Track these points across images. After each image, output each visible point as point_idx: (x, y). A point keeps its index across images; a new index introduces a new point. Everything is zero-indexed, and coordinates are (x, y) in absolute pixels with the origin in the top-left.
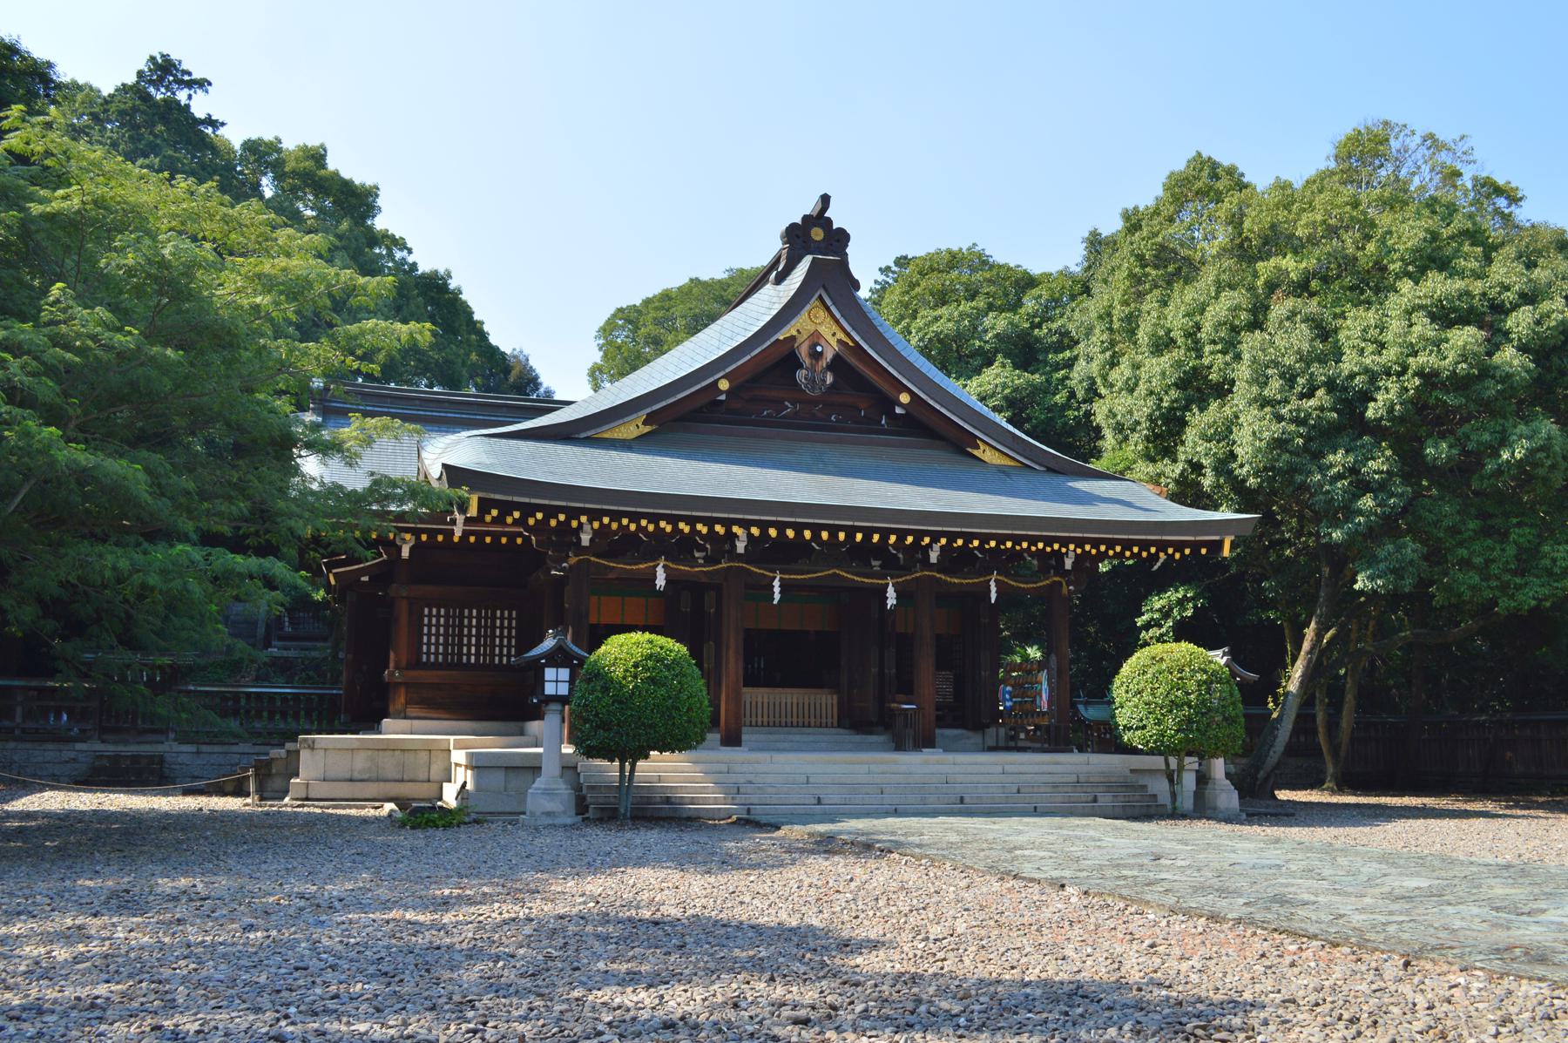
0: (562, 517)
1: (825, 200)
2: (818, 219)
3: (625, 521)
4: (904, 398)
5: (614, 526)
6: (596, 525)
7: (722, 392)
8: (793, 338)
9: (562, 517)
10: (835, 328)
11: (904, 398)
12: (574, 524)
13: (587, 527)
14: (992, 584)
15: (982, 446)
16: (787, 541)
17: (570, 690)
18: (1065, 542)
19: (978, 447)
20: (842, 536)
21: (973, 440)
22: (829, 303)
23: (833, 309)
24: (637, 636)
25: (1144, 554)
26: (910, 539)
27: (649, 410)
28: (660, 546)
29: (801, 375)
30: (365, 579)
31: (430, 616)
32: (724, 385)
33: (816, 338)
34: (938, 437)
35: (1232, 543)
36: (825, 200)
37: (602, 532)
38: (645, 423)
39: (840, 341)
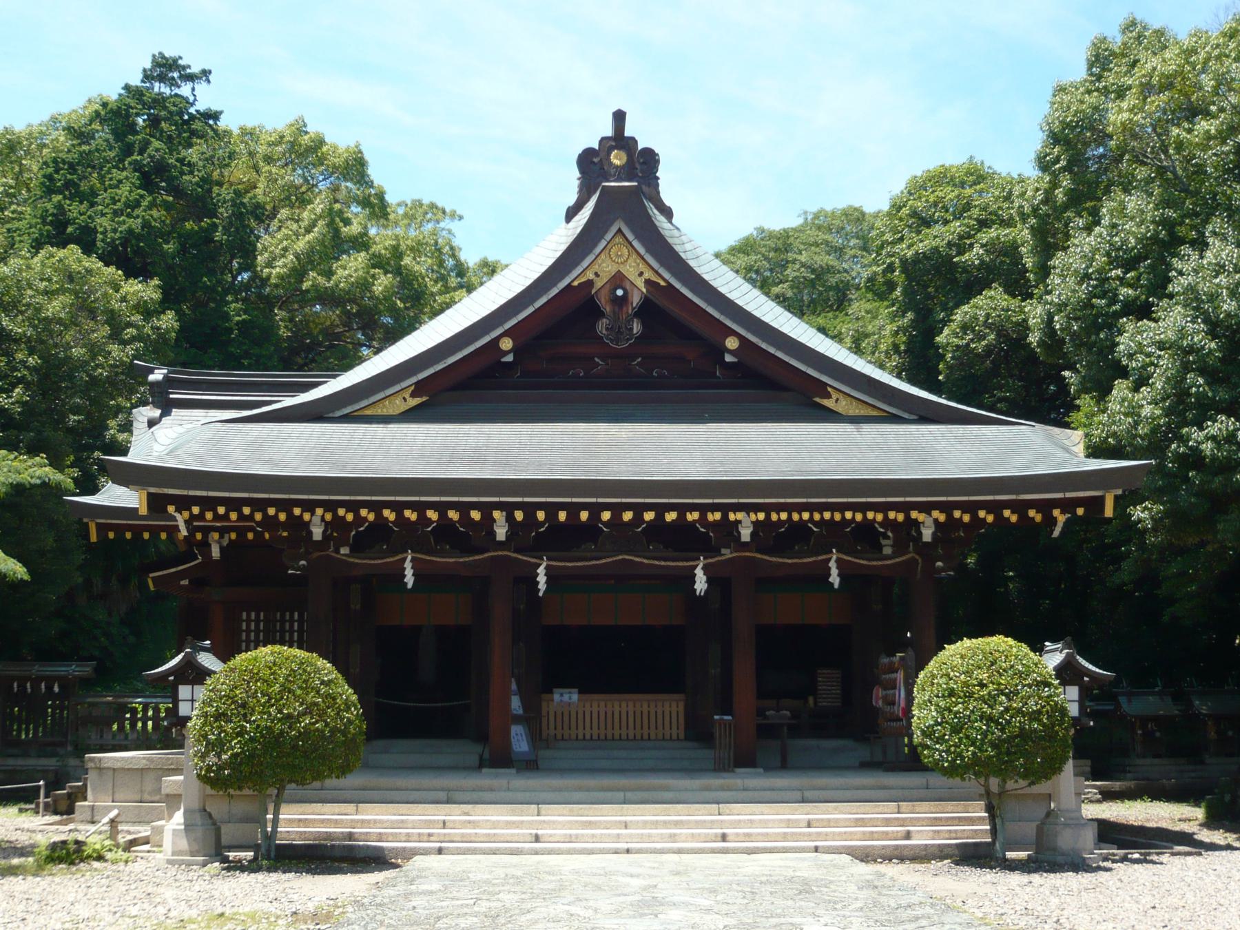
1: (619, 117)
2: (619, 139)
3: (271, 511)
4: (732, 343)
7: (506, 353)
8: (590, 283)
10: (642, 267)
11: (732, 343)
14: (832, 564)
15: (835, 395)
16: (564, 523)
18: (310, 506)
19: (829, 396)
20: (541, 515)
21: (822, 389)
22: (630, 237)
23: (636, 244)
27: (414, 380)
28: (834, 534)
29: (602, 326)
30: (185, 582)
31: (249, 621)
32: (507, 344)
33: (618, 279)
34: (777, 385)
35: (1117, 498)
36: (619, 117)
37: (336, 524)
38: (413, 395)
39: (648, 282)
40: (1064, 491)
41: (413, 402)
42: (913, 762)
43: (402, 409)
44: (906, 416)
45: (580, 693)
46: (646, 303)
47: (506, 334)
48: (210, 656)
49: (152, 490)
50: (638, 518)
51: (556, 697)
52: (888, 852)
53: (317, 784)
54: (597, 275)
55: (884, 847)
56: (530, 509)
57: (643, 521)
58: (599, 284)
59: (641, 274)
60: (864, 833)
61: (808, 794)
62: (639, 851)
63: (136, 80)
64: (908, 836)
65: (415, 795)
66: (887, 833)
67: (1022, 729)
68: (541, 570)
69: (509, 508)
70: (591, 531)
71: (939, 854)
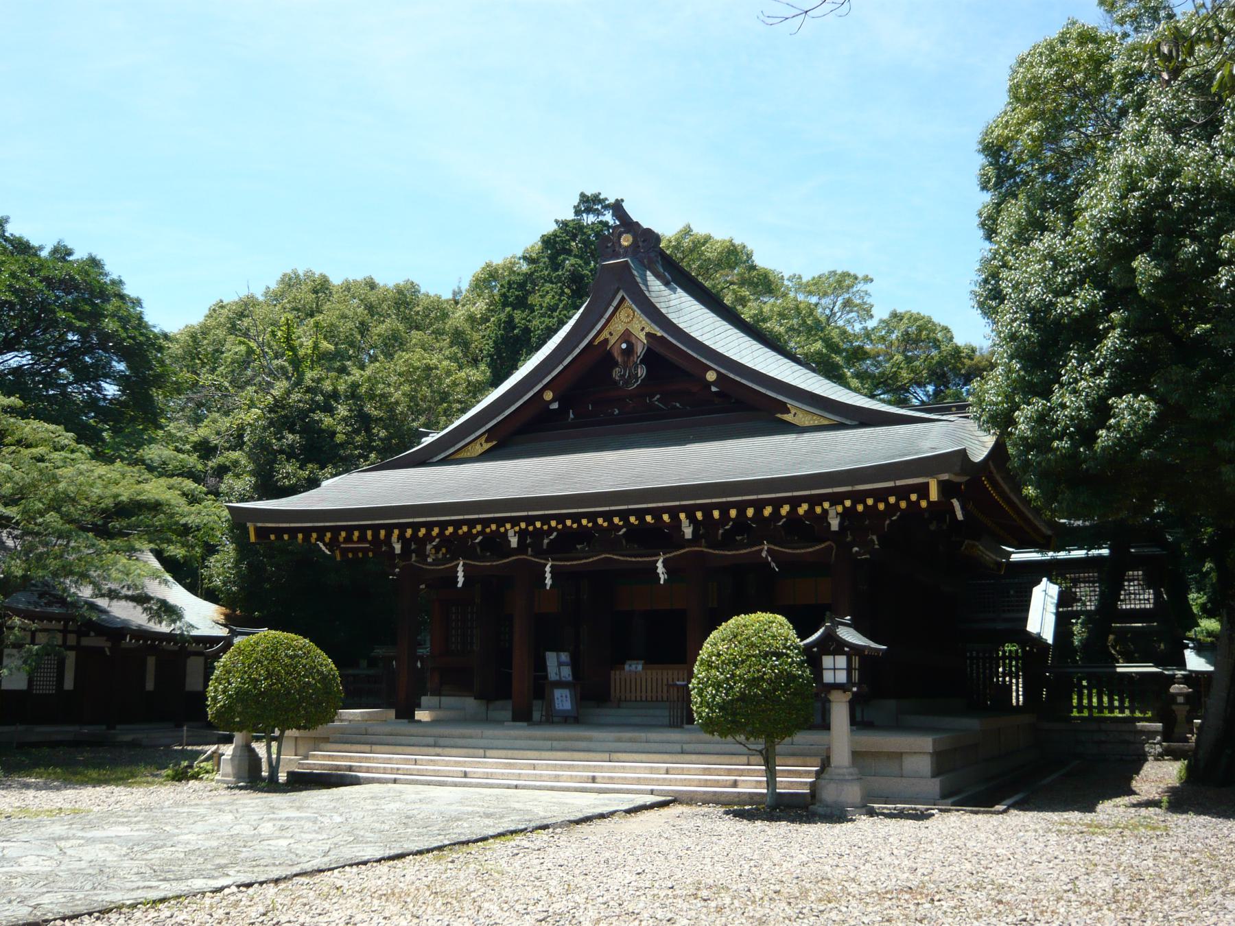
0: (848, 503)
4: (711, 376)
5: (881, 506)
6: (517, 529)
8: (606, 341)
9: (870, 502)
11: (711, 376)
12: (818, 510)
13: (832, 513)
17: (541, 666)
19: (788, 411)
20: (716, 514)
24: (264, 632)
25: (860, 508)
26: (423, 531)
29: (616, 373)
33: (627, 336)
37: (846, 515)
38: (486, 441)
39: (648, 335)
40: (894, 480)
41: (487, 446)
42: (683, 718)
43: (480, 452)
44: (848, 422)
45: (646, 663)
46: (649, 352)
47: (718, 373)
48: (851, 630)
49: (259, 525)
50: (776, 511)
51: (627, 667)
52: (708, 797)
53: (788, 739)
54: (611, 334)
55: (705, 793)
56: (707, 509)
57: (730, 519)
58: (612, 341)
59: (643, 329)
60: (700, 780)
61: (685, 747)
62: (524, 787)
63: (570, 215)
64: (735, 784)
65: (414, 740)
66: (718, 781)
67: (743, 694)
68: (660, 564)
69: (690, 511)
70: (583, 535)
71: (708, 799)
